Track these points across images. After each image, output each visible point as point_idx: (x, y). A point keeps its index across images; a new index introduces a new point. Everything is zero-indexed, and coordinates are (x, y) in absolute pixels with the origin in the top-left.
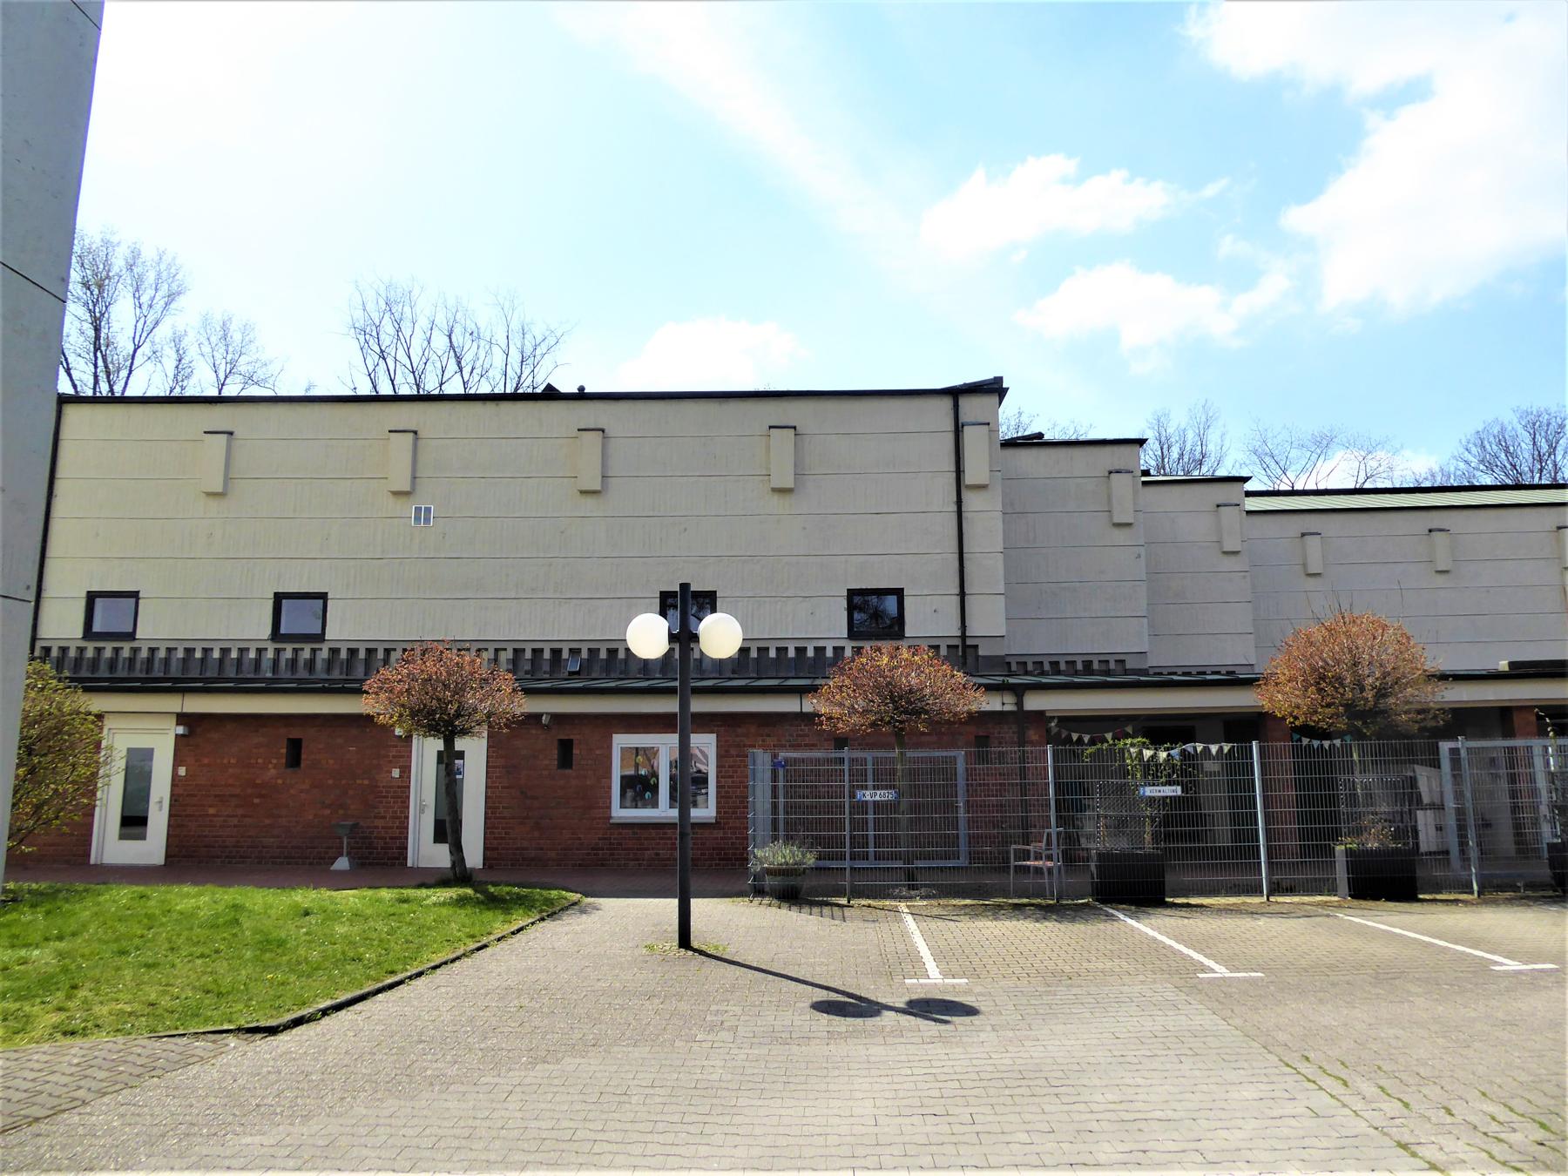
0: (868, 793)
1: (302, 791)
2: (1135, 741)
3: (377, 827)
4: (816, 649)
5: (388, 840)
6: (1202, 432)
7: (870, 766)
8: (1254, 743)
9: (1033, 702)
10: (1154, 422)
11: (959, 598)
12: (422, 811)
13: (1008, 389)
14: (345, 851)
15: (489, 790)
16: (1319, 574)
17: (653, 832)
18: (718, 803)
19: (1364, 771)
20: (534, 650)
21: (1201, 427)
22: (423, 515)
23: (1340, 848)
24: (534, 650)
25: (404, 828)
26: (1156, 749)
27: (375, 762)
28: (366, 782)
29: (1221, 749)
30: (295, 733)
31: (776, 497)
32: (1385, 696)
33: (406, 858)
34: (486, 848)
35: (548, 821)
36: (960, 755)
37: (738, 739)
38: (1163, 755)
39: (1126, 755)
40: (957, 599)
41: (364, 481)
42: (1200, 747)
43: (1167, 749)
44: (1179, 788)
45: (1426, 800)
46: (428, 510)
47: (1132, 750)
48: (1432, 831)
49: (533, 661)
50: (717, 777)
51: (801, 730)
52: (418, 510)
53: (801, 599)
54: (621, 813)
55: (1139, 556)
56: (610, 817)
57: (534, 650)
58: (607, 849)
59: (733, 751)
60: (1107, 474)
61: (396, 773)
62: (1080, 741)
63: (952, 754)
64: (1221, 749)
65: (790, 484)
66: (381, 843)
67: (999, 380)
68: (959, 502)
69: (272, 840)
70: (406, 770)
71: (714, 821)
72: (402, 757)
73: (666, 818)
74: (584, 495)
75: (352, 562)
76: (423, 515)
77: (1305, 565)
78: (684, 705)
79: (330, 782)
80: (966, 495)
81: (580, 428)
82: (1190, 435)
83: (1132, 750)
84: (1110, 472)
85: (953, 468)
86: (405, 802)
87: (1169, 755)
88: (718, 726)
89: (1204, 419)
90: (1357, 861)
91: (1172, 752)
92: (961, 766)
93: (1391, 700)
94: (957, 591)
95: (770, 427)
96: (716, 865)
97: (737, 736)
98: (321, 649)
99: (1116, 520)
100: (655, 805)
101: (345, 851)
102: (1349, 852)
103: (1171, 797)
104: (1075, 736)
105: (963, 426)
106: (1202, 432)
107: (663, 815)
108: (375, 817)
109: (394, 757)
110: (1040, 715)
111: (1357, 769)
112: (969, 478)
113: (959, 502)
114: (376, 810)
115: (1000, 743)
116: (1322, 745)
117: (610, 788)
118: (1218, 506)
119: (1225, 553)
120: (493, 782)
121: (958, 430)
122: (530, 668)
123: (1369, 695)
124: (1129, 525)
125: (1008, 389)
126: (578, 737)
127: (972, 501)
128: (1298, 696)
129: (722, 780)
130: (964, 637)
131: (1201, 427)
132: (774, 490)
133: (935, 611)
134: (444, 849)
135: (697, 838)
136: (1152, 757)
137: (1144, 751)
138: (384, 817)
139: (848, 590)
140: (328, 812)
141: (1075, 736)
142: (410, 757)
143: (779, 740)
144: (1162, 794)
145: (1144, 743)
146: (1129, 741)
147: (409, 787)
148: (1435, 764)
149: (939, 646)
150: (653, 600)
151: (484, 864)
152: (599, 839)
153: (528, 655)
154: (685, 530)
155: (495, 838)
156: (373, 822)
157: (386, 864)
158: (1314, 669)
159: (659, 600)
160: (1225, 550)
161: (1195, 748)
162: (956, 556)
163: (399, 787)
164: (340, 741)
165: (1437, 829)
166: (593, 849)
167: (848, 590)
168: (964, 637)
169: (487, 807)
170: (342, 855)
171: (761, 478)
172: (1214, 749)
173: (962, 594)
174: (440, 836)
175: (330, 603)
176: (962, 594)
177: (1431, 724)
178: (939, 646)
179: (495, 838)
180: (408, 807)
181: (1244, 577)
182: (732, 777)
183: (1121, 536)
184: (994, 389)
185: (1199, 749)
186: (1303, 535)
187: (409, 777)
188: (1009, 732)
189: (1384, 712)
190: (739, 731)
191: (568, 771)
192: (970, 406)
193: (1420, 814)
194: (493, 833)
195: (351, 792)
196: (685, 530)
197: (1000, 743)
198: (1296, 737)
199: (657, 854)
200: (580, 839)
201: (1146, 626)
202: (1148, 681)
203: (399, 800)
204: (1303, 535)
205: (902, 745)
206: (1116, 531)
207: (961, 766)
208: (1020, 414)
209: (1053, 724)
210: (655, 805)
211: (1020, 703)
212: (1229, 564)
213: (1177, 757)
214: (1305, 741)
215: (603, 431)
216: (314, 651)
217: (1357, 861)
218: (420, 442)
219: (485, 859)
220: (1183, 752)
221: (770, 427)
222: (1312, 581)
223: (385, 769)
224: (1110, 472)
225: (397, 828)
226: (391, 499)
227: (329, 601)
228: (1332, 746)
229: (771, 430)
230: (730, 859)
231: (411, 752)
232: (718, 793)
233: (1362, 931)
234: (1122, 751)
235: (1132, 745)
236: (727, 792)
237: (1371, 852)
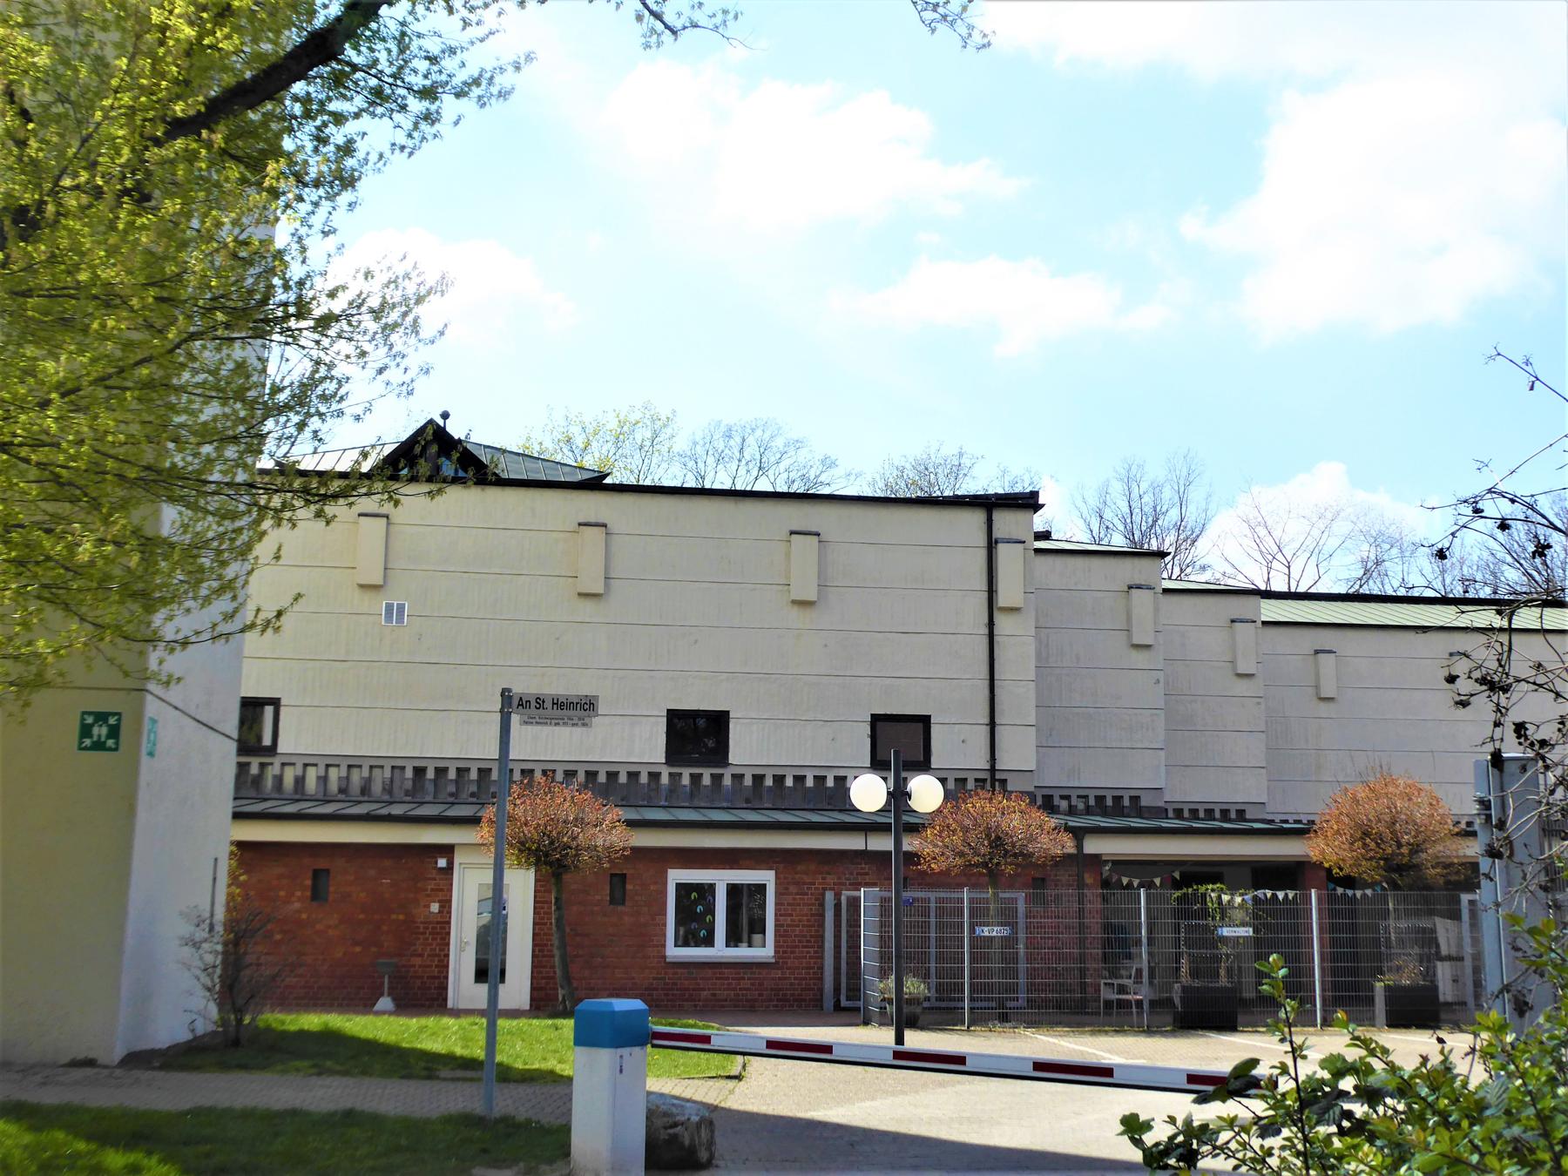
0: (986, 929)
1: (330, 927)
2: (1215, 887)
3: (414, 966)
4: (836, 778)
5: (425, 979)
6: (1182, 490)
7: (933, 905)
8: (1313, 891)
9: (1093, 846)
10: (1122, 471)
11: (988, 728)
12: (462, 950)
13: (1043, 506)
14: (386, 989)
15: (537, 927)
16: (1332, 699)
17: (709, 973)
18: (776, 941)
19: (1398, 918)
20: (459, 770)
21: (1182, 483)
22: (394, 613)
23: (1379, 985)
24: (480, 770)
25: (445, 967)
26: (1232, 894)
27: (412, 895)
28: (401, 917)
29: (1286, 895)
30: (322, 864)
31: (796, 608)
32: (1417, 852)
33: (445, 1000)
34: (533, 989)
35: (599, 959)
36: (1021, 896)
37: (797, 876)
38: (1238, 900)
39: (1208, 899)
40: (985, 730)
41: (324, 569)
42: (1269, 893)
43: (1241, 895)
44: (1251, 930)
45: (1444, 951)
46: (401, 608)
47: (1213, 895)
48: (1449, 983)
49: (435, 781)
50: (776, 915)
51: (862, 869)
52: (389, 608)
53: (822, 723)
54: (674, 952)
55: (1158, 681)
56: (664, 957)
57: (459, 770)
58: (662, 989)
59: (793, 889)
60: (1126, 589)
61: (435, 907)
62: (1130, 886)
63: (1013, 896)
64: (1286, 895)
65: (813, 598)
66: (418, 982)
67: (1034, 495)
68: (991, 624)
69: (295, 980)
70: (446, 904)
71: (773, 961)
72: (442, 890)
73: (722, 957)
74: (582, 599)
75: (311, 664)
76: (394, 613)
77: (1317, 687)
78: (898, 843)
79: (361, 916)
80: (999, 619)
81: (581, 521)
82: (1168, 494)
83: (1213, 895)
84: (1130, 587)
85: (985, 587)
86: (444, 939)
87: (1243, 900)
88: (777, 862)
89: (1185, 472)
90: (1393, 994)
91: (1246, 897)
92: (1021, 907)
93: (1424, 856)
94: (987, 720)
95: (792, 533)
96: (774, 1006)
97: (796, 873)
98: (272, 764)
99: (1136, 641)
100: (709, 941)
101: (386, 989)
102: (1387, 988)
103: (1244, 937)
104: (1125, 881)
105: (996, 542)
106: (1182, 490)
107: (720, 954)
108: (412, 955)
109: (432, 890)
110: (1096, 859)
111: (1392, 915)
112: (1003, 600)
113: (991, 624)
114: (413, 948)
115: (1056, 885)
116: (1355, 895)
117: (665, 925)
118: (1233, 621)
119: (1239, 675)
120: (444, 928)
121: (991, 545)
122: (454, 790)
123: (1405, 850)
124: (1148, 647)
125: (1043, 506)
126: (631, 871)
127: (1003, 624)
128: (1344, 850)
129: (782, 918)
130: (993, 770)
131: (1182, 483)
132: (794, 602)
133: (963, 741)
134: (483, 989)
135: (753, 979)
136: (1229, 902)
137: (1223, 896)
138: (421, 955)
139: (872, 715)
140: (358, 949)
141: (1125, 881)
142: (451, 890)
143: (839, 878)
144: (1237, 934)
145: (1222, 889)
146: (1210, 886)
147: (449, 923)
148: (1455, 915)
149: (966, 779)
150: (660, 719)
151: (531, 1005)
152: (654, 979)
153: (474, 775)
154: (696, 642)
155: (543, 978)
156: (409, 960)
157: (422, 1006)
158: (1358, 826)
159: (665, 719)
160: (1239, 672)
161: (1265, 894)
162: (987, 683)
163: (438, 923)
164: (372, 873)
165: (1454, 981)
166: (646, 989)
167: (872, 715)
168: (993, 770)
169: (534, 945)
170: (382, 995)
171: (780, 588)
172: (1281, 895)
173: (992, 724)
174: (481, 975)
175: (283, 711)
176: (992, 724)
177: (1454, 878)
178: (966, 779)
179: (543, 978)
180: (448, 944)
181: (1259, 703)
182: (791, 915)
183: (1139, 658)
184: (1028, 502)
185: (1269, 895)
186: (1317, 652)
187: (450, 912)
188: (1064, 876)
189: (1417, 867)
190: (799, 868)
191: (620, 908)
192: (1006, 522)
193: (1439, 964)
194: (541, 972)
195: (385, 928)
196: (696, 642)
197: (1056, 885)
198: (1331, 886)
199: (714, 995)
200: (633, 978)
201: (1163, 758)
202: (1229, 829)
203: (439, 937)
204: (1317, 652)
205: (995, 885)
206: (1134, 654)
207: (1021, 907)
208: (961, 455)
209: (1107, 868)
210: (709, 941)
211: (1079, 846)
212: (1242, 687)
213: (1250, 902)
214: (1340, 890)
215: (605, 526)
216: (263, 766)
217: (1393, 994)
218: (391, 527)
219: (532, 999)
220: (1255, 899)
221: (792, 533)
222: (1323, 705)
223: (422, 904)
224: (1130, 587)
225: (436, 966)
226: (357, 592)
227: (282, 708)
228: (1364, 895)
229: (793, 536)
230: (795, 1000)
231: (452, 885)
232: (776, 931)
233: (1407, 1041)
234: (1204, 896)
235: (1213, 890)
236: (785, 931)
237: (1404, 988)
